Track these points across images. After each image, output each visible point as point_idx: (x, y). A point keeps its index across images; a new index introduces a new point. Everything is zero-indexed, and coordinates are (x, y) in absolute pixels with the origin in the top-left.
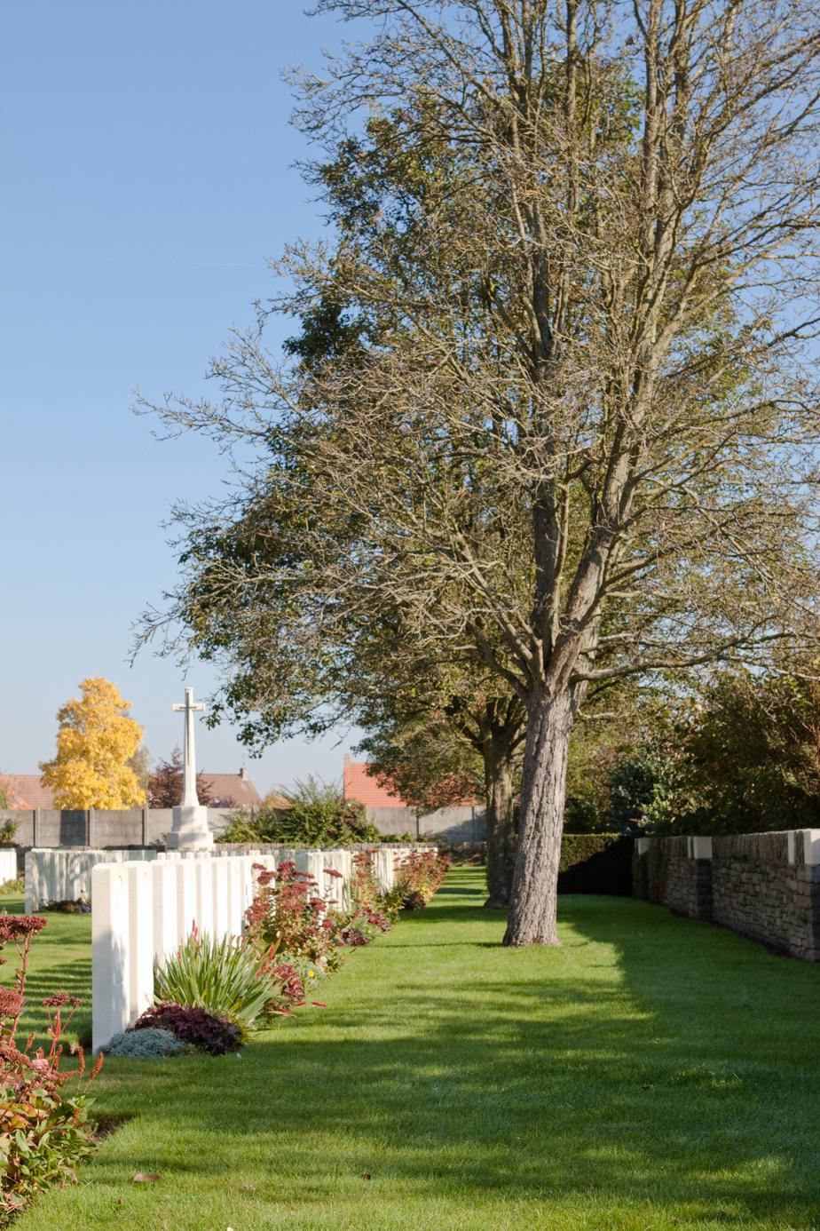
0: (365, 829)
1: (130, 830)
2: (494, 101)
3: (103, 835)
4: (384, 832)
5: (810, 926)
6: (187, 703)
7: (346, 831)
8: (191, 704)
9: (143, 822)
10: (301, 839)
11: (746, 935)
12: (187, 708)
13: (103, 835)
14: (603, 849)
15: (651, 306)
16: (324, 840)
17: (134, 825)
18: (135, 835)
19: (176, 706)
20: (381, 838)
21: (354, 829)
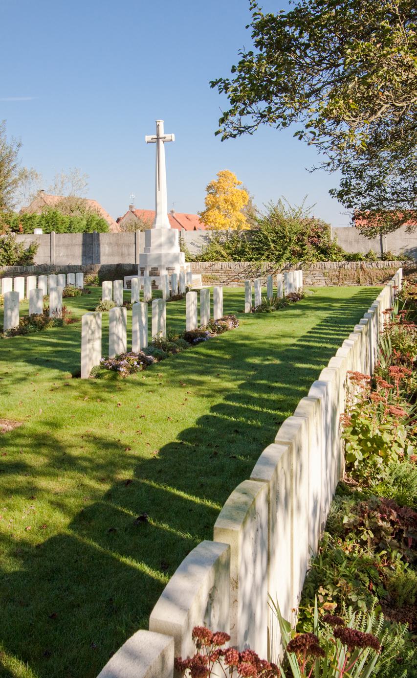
0: (328, 248)
1: (125, 250)
4: (348, 250)
6: (158, 135)
8: (162, 135)
9: (135, 244)
10: (268, 257)
17: (128, 246)
18: (129, 255)
19: (148, 138)
20: (344, 256)
21: (318, 248)
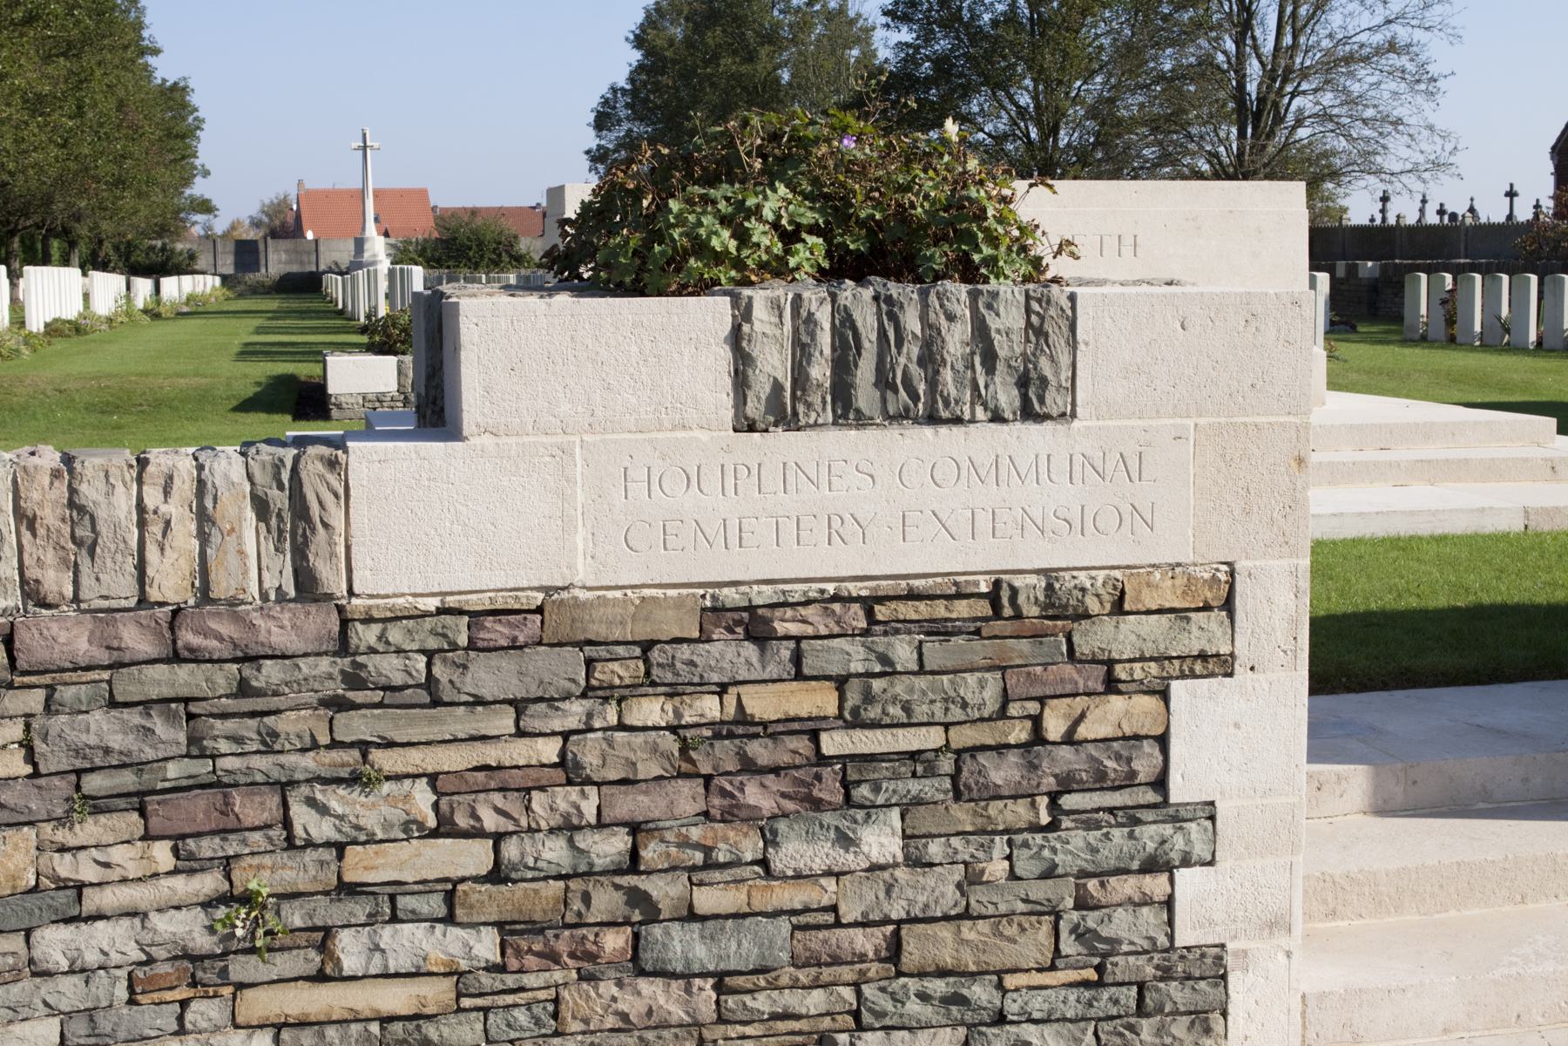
0: (521, 256)
1: (305, 258)
2: (963, 698)
3: (280, 262)
5: (41, 447)
7: (505, 258)
8: (368, 143)
9: (317, 251)
11: (106, 409)
12: (365, 148)
13: (280, 262)
14: (872, 278)
15: (584, 1033)
16: (488, 267)
17: (309, 253)
18: (309, 263)
21: (511, 256)
